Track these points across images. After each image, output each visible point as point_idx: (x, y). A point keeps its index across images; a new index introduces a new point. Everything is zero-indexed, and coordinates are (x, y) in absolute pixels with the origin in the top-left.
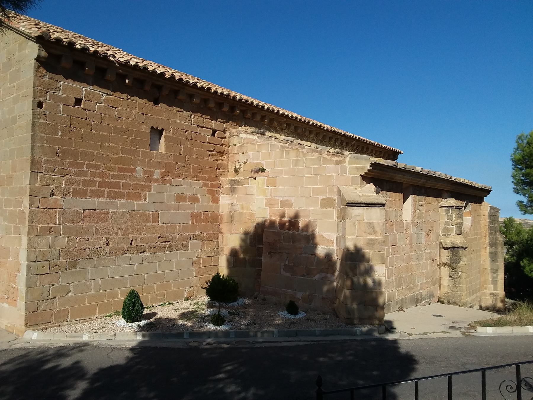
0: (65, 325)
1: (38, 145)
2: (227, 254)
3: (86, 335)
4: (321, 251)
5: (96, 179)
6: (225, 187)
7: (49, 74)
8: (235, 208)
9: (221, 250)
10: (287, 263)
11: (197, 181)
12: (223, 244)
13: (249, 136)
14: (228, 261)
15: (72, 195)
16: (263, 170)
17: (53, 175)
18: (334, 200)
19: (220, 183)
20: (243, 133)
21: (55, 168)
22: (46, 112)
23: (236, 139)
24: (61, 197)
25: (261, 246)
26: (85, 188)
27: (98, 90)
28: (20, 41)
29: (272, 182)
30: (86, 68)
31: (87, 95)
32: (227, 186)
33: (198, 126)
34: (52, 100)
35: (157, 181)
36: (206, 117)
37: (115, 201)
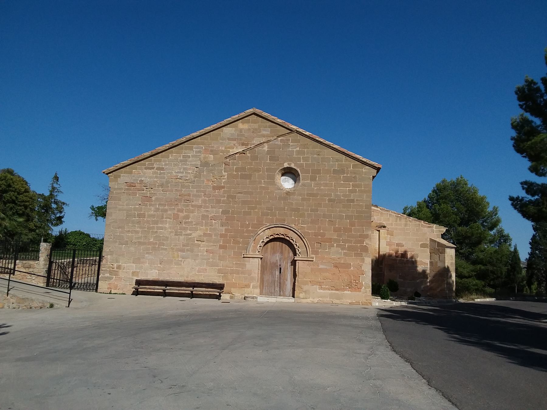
4: (420, 268)
10: (401, 274)
16: (384, 227)
18: (428, 244)
25: (381, 266)
29: (391, 233)
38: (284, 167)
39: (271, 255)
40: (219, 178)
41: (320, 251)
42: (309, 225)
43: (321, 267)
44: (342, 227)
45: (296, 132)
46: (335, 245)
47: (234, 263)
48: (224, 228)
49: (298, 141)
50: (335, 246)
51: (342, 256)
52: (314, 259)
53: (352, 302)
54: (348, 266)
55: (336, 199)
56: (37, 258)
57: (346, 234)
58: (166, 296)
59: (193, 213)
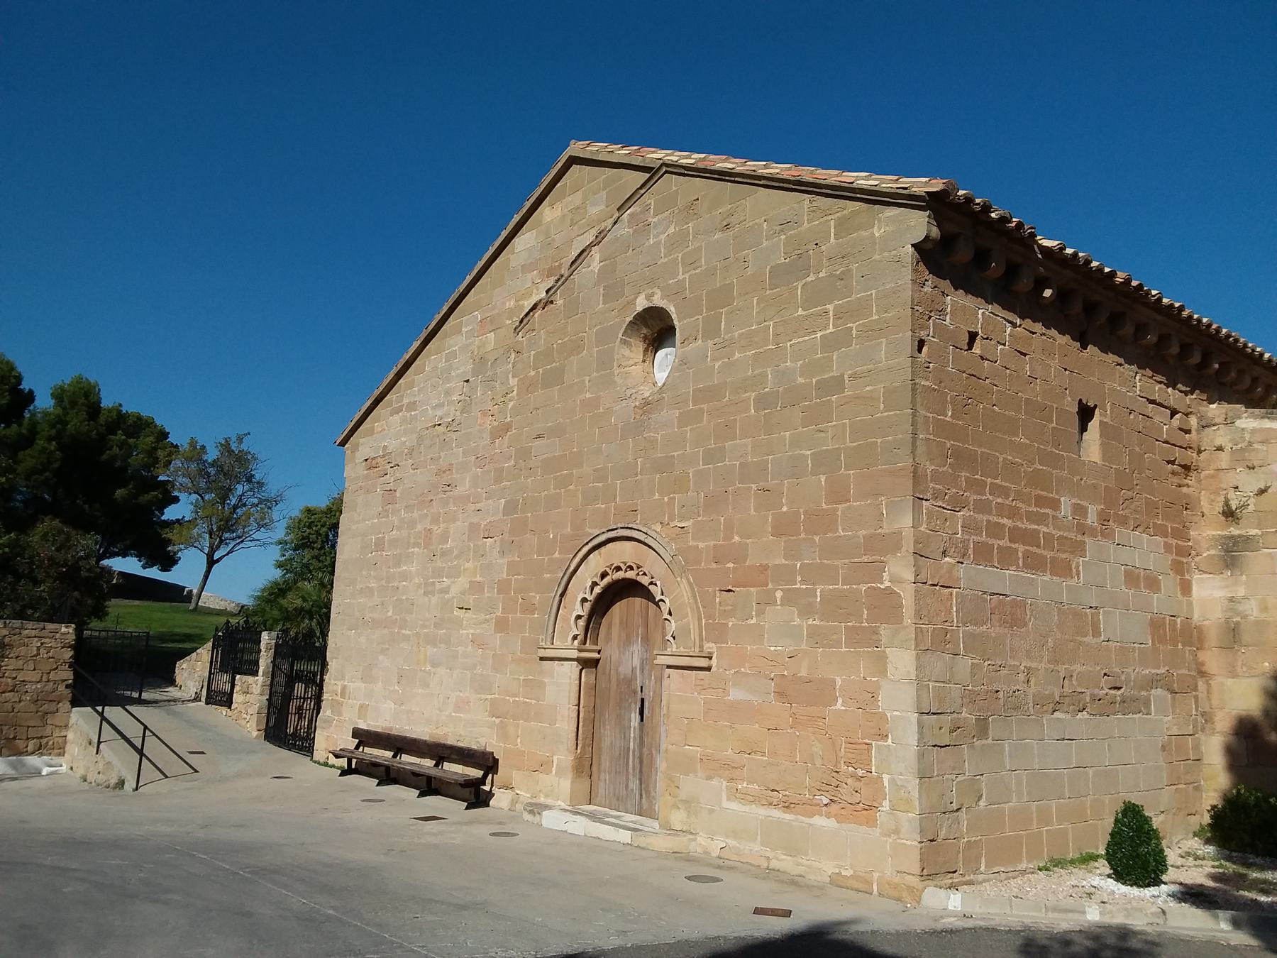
0: (981, 883)
1: (921, 436)
2: (1225, 730)
3: (1093, 907)
5: (1005, 521)
6: (1205, 555)
7: (933, 278)
8: (1241, 608)
9: (1206, 720)
11: (1154, 537)
12: (1211, 704)
13: (1269, 423)
14: (1230, 751)
15: (972, 556)
17: (943, 508)
19: (1190, 544)
20: (1246, 418)
21: (947, 491)
22: (930, 363)
23: (1221, 432)
24: (957, 560)
26: (990, 541)
27: (1000, 315)
28: (845, 212)
30: (994, 264)
31: (984, 325)
32: (1213, 552)
33: (1148, 399)
34: (938, 335)
35: (1093, 532)
36: (1159, 378)
37: (1033, 576)
38: (635, 313)
39: (619, 648)
40: (503, 399)
41: (730, 624)
42: (699, 519)
43: (735, 694)
44: (801, 510)
45: (666, 172)
46: (779, 594)
47: (522, 678)
48: (506, 560)
49: (691, 209)
50: (779, 603)
51: (803, 647)
52: (714, 662)
53: (839, 874)
54: (822, 692)
55: (781, 389)
56: (255, 673)
57: (817, 538)
58: (436, 792)
59: (454, 522)
